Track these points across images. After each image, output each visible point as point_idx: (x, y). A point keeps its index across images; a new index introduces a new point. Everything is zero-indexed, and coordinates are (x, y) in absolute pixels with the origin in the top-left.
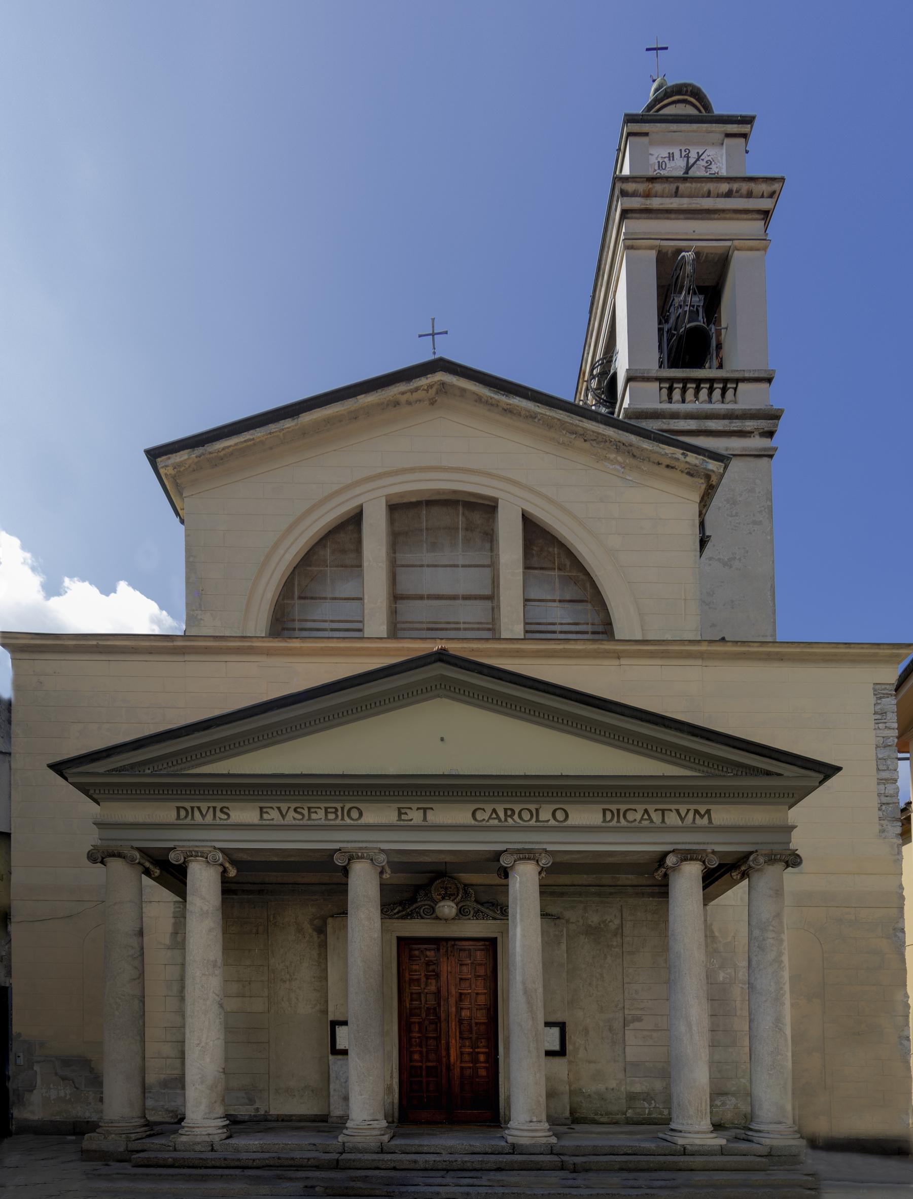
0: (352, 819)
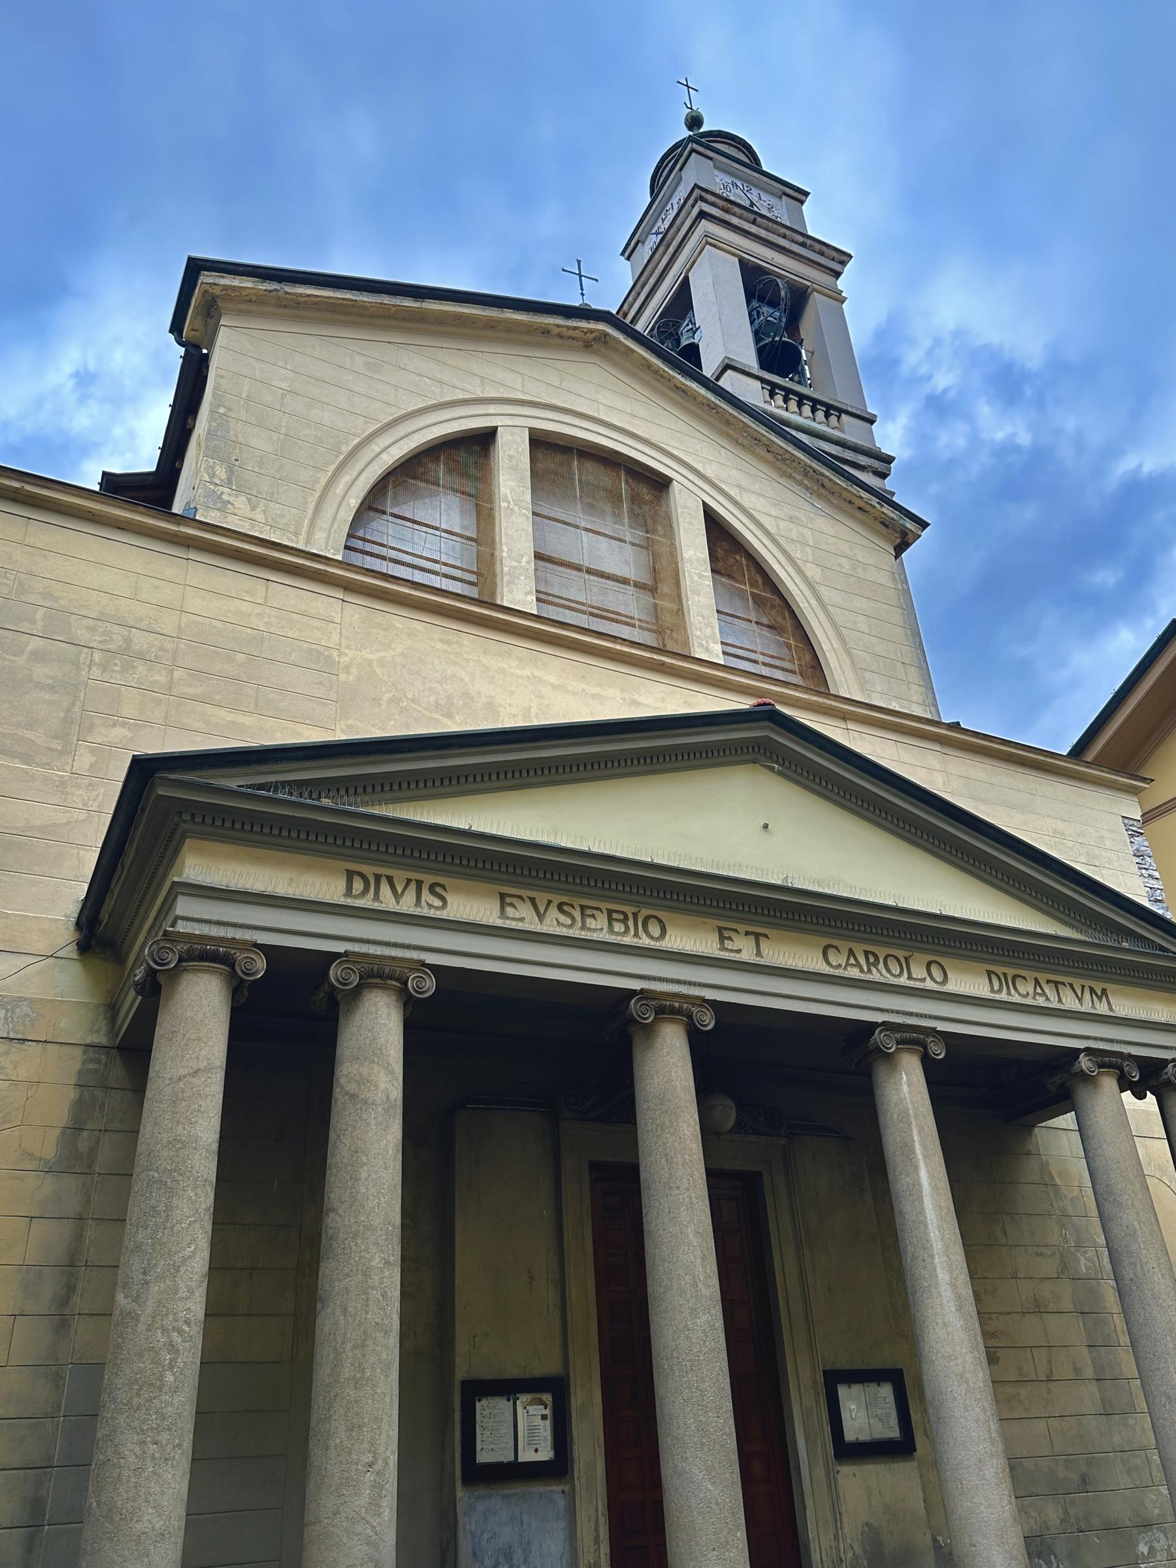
0: (652, 938)
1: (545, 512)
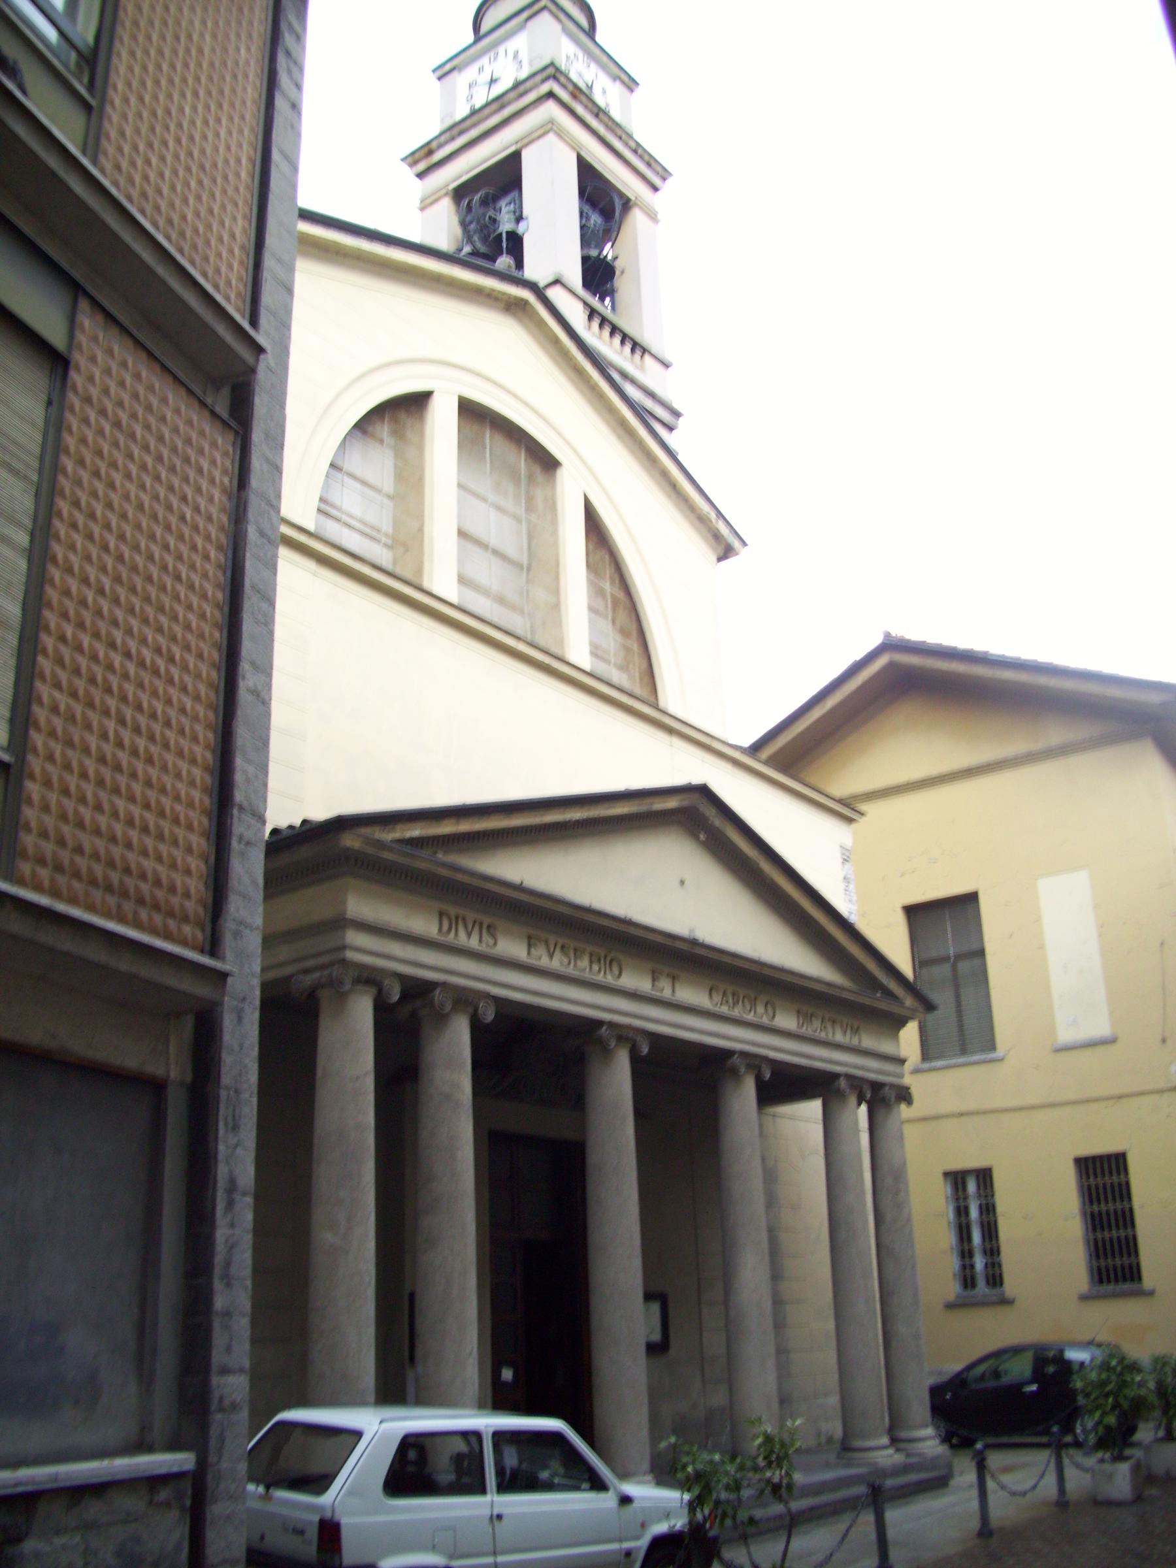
1: (472, 485)
